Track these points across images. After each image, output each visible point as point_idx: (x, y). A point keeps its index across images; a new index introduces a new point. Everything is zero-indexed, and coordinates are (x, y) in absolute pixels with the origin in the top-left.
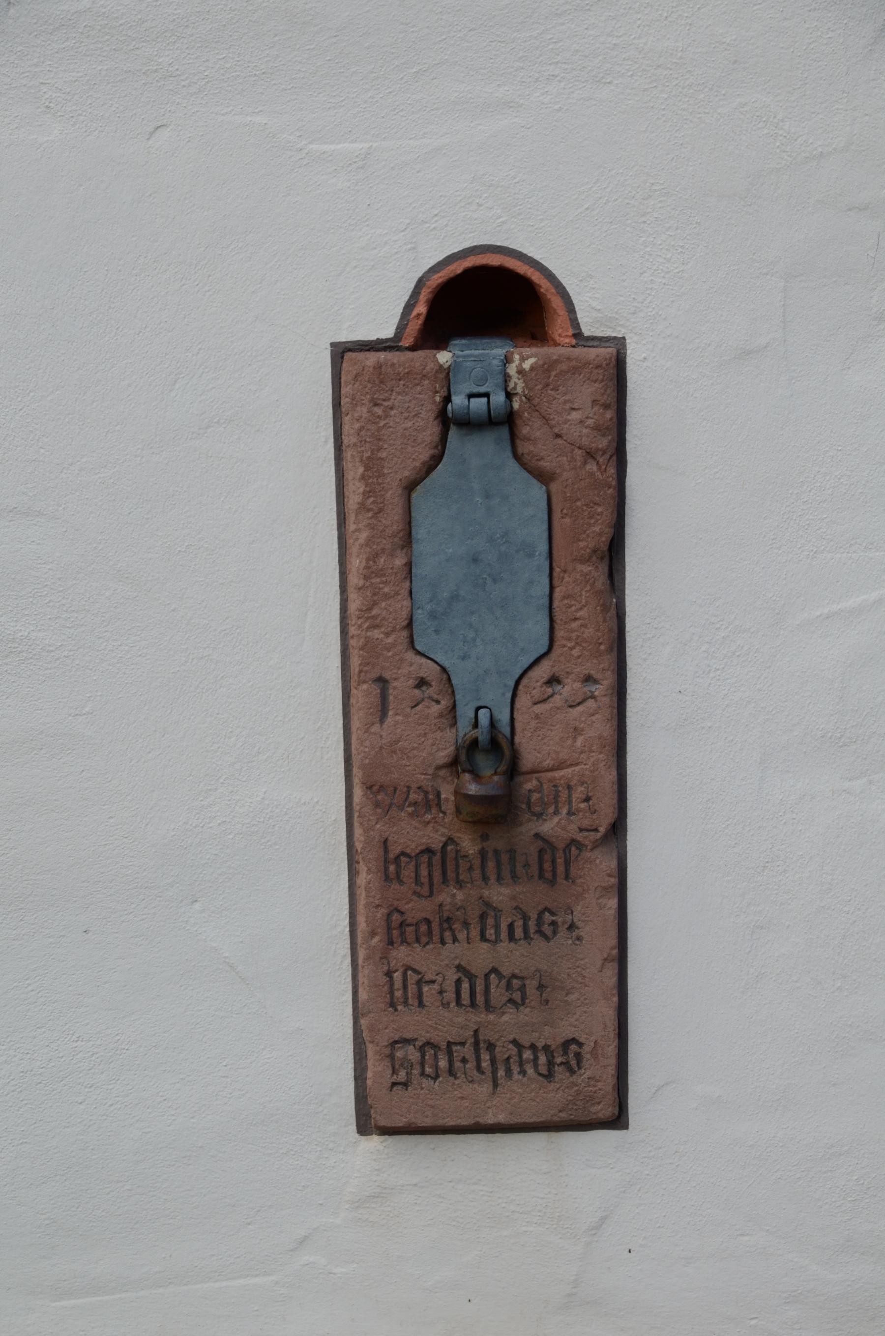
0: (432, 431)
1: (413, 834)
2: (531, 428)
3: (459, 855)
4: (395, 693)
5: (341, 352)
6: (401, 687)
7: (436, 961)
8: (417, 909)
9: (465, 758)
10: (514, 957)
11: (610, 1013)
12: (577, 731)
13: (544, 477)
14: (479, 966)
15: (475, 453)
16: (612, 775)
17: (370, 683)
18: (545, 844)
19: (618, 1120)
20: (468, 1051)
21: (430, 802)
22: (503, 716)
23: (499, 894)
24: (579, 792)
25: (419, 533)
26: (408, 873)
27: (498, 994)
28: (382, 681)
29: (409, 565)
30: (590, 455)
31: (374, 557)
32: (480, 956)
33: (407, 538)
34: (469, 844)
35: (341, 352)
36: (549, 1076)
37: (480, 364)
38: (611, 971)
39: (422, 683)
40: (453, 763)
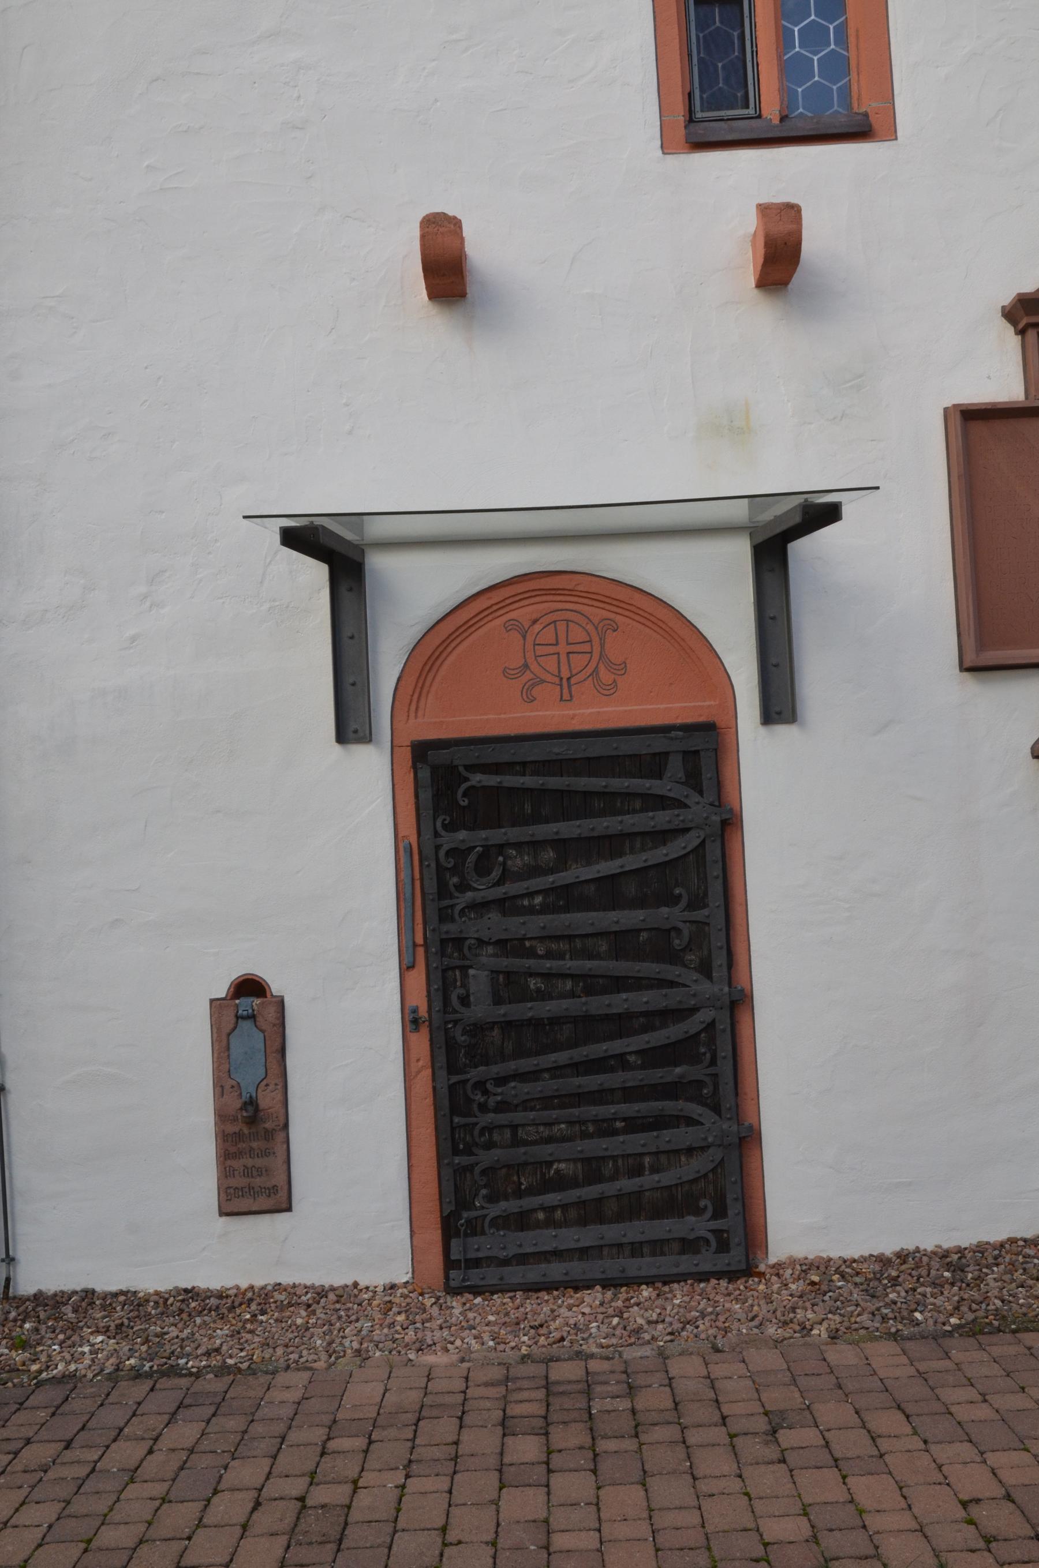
0: (234, 1020)
1: (231, 1128)
2: (259, 1019)
3: (244, 1134)
4: (709, 1289)
5: (212, 1001)
6: (227, 1087)
7: (237, 1164)
8: (232, 1150)
9: (245, 1106)
10: (259, 1162)
11: (286, 1178)
12: (274, 1099)
13: (263, 1031)
14: (250, 1165)
15: (246, 1025)
16: (283, 1111)
17: (220, 1088)
18: (266, 1131)
19: (289, 1209)
20: (247, 1190)
21: (235, 1120)
22: (254, 1095)
23: (255, 1145)
24: (275, 1115)
25: (232, 1046)
26: (230, 1139)
27: (255, 1173)
28: (222, 1087)
29: (229, 1056)
30: (274, 1025)
31: (219, 1054)
32: (250, 1162)
33: (228, 1048)
34: (246, 1131)
35: (212, 1001)
36: (269, 1196)
37: (246, 1004)
38: (285, 1167)
39: (233, 1087)
40: (241, 1109)
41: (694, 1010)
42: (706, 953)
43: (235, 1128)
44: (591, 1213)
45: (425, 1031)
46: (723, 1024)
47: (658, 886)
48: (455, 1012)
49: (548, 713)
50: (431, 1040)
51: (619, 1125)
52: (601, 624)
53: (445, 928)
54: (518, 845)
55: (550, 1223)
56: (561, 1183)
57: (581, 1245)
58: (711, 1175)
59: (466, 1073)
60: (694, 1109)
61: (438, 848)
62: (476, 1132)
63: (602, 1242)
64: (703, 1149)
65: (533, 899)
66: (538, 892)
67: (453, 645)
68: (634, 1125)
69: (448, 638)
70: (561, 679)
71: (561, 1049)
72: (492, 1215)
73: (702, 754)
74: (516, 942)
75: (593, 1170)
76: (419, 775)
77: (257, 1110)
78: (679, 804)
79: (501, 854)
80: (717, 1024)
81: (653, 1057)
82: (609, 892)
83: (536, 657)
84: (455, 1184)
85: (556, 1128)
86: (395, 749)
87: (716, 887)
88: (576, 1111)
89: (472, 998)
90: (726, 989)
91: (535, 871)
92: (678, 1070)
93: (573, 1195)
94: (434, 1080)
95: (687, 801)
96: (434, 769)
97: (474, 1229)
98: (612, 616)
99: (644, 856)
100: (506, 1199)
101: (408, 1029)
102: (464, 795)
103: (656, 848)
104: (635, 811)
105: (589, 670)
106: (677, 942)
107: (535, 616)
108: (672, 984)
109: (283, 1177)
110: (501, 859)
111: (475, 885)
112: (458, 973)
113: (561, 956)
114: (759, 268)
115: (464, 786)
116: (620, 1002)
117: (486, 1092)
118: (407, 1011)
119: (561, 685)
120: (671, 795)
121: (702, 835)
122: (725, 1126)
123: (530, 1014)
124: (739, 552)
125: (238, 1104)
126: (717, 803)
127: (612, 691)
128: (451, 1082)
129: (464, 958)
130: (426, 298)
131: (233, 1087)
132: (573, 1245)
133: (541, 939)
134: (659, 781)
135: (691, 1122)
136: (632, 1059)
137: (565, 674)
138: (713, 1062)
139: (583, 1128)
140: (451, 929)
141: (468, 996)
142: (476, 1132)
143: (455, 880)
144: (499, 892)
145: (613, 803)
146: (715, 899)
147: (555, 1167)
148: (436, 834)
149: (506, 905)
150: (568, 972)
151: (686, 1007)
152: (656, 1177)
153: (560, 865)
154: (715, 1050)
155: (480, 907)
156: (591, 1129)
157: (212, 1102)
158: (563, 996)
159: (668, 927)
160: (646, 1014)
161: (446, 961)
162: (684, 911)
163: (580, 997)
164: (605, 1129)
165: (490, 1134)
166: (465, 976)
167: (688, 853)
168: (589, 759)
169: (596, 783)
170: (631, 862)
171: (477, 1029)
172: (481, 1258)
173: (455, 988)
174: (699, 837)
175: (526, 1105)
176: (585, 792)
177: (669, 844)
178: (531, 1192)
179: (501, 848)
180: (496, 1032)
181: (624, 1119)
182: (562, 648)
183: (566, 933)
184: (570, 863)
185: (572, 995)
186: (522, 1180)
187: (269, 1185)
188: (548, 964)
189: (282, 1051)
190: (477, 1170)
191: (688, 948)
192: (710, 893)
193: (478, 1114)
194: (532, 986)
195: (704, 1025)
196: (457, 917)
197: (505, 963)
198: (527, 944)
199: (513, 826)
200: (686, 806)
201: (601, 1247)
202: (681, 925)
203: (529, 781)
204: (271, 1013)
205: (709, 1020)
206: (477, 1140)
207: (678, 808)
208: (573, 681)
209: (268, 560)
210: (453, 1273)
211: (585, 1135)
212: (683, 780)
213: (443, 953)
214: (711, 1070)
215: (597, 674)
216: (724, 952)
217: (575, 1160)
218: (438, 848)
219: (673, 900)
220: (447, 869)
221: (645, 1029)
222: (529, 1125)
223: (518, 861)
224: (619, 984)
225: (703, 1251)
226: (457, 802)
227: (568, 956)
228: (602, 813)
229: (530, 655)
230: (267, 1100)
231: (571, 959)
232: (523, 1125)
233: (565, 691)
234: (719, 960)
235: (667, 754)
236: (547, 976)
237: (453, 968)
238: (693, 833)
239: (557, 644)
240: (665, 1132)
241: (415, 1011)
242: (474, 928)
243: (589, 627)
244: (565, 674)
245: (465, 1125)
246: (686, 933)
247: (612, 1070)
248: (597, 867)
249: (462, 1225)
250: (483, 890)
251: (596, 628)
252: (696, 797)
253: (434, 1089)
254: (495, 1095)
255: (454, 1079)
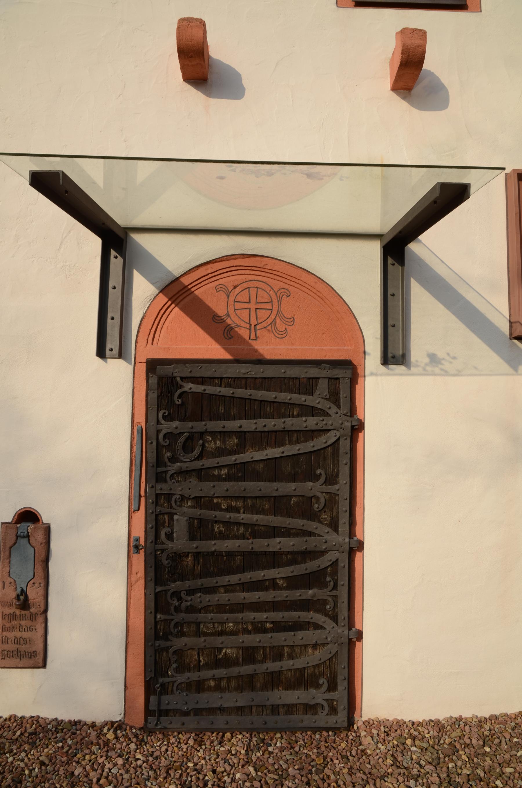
0: (15, 538)
8: (8, 625)
10: (26, 635)
15: (23, 542)
18: (31, 614)
20: (16, 653)
21: (11, 605)
22: (25, 589)
23: (23, 623)
24: (38, 604)
26: (7, 618)
29: (10, 561)
36: (31, 658)
37: (23, 527)
41: (325, 552)
42: (335, 514)
44: (248, 683)
45: (142, 552)
46: (344, 563)
47: (305, 467)
48: (163, 543)
49: (240, 347)
50: (145, 561)
51: (268, 625)
52: (280, 292)
53: (159, 486)
54: (213, 434)
55: (218, 688)
56: (227, 662)
57: (238, 704)
58: (328, 663)
59: (167, 585)
60: (319, 618)
61: (158, 431)
62: (172, 625)
63: (252, 704)
64: (324, 645)
65: (221, 470)
66: (224, 466)
67: (181, 298)
68: (279, 627)
69: (177, 293)
70: (250, 325)
71: (234, 573)
72: (179, 681)
73: (341, 380)
74: (207, 499)
75: (249, 655)
76: (150, 382)
78: (324, 413)
79: (201, 438)
80: (339, 563)
81: (294, 583)
82: (273, 470)
83: (235, 309)
84: (155, 660)
85: (226, 625)
86: (137, 364)
87: (345, 471)
88: (240, 615)
89: (175, 535)
90: (347, 540)
91: (224, 452)
92: (311, 592)
93: (235, 671)
94: (145, 589)
95: (330, 412)
96: (160, 378)
97: (165, 689)
98: (287, 286)
99: (297, 447)
100: (189, 671)
101: (132, 552)
102: (180, 397)
103: (306, 442)
104: (293, 416)
105: (270, 321)
106: (316, 506)
107: (236, 284)
108: (311, 534)
109: (41, 645)
110: (201, 442)
111: (182, 459)
112: (166, 517)
113: (236, 510)
114: (394, 79)
115: (179, 391)
116: (276, 544)
117: (180, 599)
118: (132, 540)
119: (250, 329)
120: (319, 406)
121: (338, 434)
122: (340, 631)
123: (213, 549)
124: (375, 249)
125: (14, 595)
126: (349, 414)
127: (284, 336)
128: (157, 590)
129: (171, 507)
130: (182, 80)
131: (11, 583)
132: (232, 705)
133: (225, 498)
134: (311, 397)
135: (317, 627)
136: (280, 582)
137: (253, 322)
138: (335, 588)
139: (245, 626)
140: (164, 488)
141: (172, 533)
142: (172, 625)
143: (169, 454)
144: (198, 464)
145: (280, 409)
146: (344, 479)
147: (224, 651)
148: (158, 422)
149: (202, 474)
150: (242, 521)
151: (319, 550)
152: (291, 662)
153: (241, 449)
154: (337, 580)
155: (184, 474)
156: (250, 628)
158: (237, 537)
159: (311, 495)
160: (293, 553)
161: (159, 509)
162: (322, 485)
163: (248, 539)
164: (259, 628)
165: (182, 627)
166: (171, 519)
167: (328, 447)
168: (265, 378)
169: (269, 395)
170: (289, 450)
171: (178, 557)
172: (170, 710)
173: (164, 527)
174: (336, 436)
175: (206, 609)
176: (261, 401)
177: (315, 439)
178: (208, 666)
179: (202, 434)
180: (190, 558)
181: (272, 622)
182: (252, 306)
183: (242, 495)
184: (247, 448)
185: (243, 537)
186: (201, 658)
187: (32, 650)
188: (228, 515)
190: (171, 651)
191: (323, 510)
192: (340, 474)
193: (174, 613)
194: (216, 530)
195: (331, 562)
196: (168, 479)
197: (198, 512)
198: (215, 501)
199: (210, 420)
200: (328, 415)
201: (251, 707)
202: (319, 495)
203: (225, 391)
204: (38, 536)
205: (334, 559)
206: (172, 631)
207: (323, 416)
208: (258, 327)
209: (64, 235)
210: (150, 719)
211: (245, 631)
212: (328, 397)
213: (157, 503)
214: (333, 593)
215: (275, 323)
216: (348, 514)
217: (238, 648)
218: (158, 431)
219: (315, 478)
220: (164, 446)
221: (290, 563)
222: (208, 622)
223: (213, 444)
224: (275, 532)
225: (320, 713)
226: (174, 401)
227: (242, 511)
228: (271, 416)
229: (231, 308)
231: (244, 513)
232: (205, 622)
233: (253, 333)
234: (344, 520)
235: (319, 378)
236: (227, 524)
237: (164, 514)
238: (332, 433)
239: (249, 302)
240: (299, 632)
241: (137, 540)
242: (179, 488)
243: (272, 293)
244: (253, 322)
245: (165, 620)
246: (322, 500)
247: (267, 589)
248: (266, 452)
249: (158, 688)
250: (187, 462)
251: (276, 294)
252: (334, 409)
253: (145, 594)
254: (186, 601)
255: (159, 589)
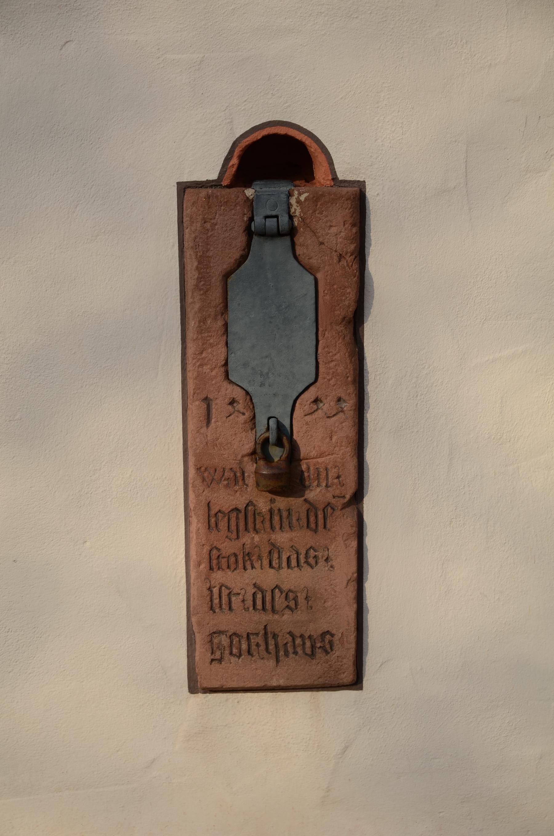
0: (241, 240)
1: (226, 499)
5: (183, 188)
7: (241, 581)
8: (228, 547)
9: (261, 451)
10: (292, 578)
13: (310, 270)
15: (272, 251)
18: (312, 507)
19: (356, 683)
20: (260, 639)
21: (237, 478)
22: (286, 422)
23: (282, 538)
24: (333, 473)
26: (223, 524)
28: (207, 400)
31: (203, 321)
35: (183, 188)
36: (312, 655)
43: (239, 500)
77: (293, 455)
125: (246, 443)
131: (232, 402)
157: (365, 509)
189: (356, 320)
230: (317, 438)
